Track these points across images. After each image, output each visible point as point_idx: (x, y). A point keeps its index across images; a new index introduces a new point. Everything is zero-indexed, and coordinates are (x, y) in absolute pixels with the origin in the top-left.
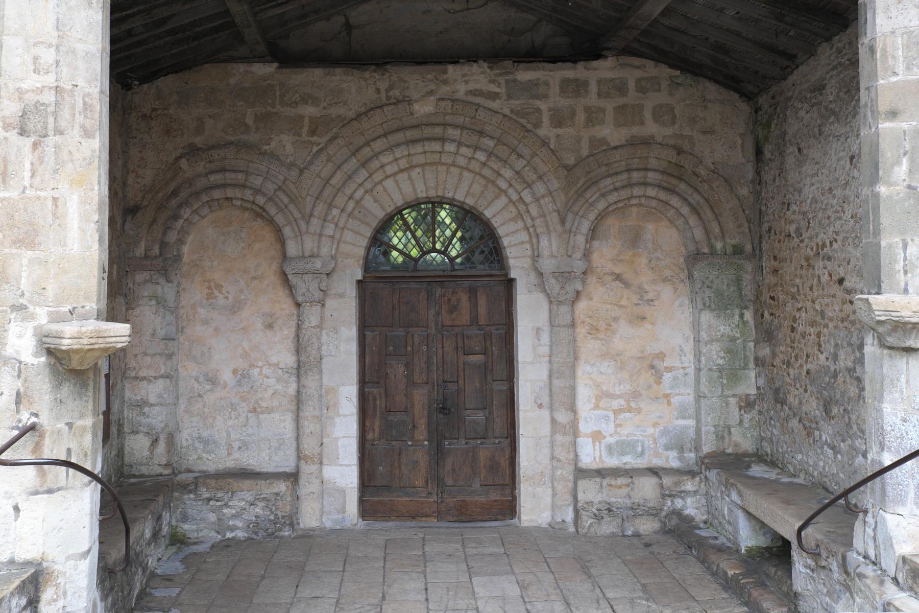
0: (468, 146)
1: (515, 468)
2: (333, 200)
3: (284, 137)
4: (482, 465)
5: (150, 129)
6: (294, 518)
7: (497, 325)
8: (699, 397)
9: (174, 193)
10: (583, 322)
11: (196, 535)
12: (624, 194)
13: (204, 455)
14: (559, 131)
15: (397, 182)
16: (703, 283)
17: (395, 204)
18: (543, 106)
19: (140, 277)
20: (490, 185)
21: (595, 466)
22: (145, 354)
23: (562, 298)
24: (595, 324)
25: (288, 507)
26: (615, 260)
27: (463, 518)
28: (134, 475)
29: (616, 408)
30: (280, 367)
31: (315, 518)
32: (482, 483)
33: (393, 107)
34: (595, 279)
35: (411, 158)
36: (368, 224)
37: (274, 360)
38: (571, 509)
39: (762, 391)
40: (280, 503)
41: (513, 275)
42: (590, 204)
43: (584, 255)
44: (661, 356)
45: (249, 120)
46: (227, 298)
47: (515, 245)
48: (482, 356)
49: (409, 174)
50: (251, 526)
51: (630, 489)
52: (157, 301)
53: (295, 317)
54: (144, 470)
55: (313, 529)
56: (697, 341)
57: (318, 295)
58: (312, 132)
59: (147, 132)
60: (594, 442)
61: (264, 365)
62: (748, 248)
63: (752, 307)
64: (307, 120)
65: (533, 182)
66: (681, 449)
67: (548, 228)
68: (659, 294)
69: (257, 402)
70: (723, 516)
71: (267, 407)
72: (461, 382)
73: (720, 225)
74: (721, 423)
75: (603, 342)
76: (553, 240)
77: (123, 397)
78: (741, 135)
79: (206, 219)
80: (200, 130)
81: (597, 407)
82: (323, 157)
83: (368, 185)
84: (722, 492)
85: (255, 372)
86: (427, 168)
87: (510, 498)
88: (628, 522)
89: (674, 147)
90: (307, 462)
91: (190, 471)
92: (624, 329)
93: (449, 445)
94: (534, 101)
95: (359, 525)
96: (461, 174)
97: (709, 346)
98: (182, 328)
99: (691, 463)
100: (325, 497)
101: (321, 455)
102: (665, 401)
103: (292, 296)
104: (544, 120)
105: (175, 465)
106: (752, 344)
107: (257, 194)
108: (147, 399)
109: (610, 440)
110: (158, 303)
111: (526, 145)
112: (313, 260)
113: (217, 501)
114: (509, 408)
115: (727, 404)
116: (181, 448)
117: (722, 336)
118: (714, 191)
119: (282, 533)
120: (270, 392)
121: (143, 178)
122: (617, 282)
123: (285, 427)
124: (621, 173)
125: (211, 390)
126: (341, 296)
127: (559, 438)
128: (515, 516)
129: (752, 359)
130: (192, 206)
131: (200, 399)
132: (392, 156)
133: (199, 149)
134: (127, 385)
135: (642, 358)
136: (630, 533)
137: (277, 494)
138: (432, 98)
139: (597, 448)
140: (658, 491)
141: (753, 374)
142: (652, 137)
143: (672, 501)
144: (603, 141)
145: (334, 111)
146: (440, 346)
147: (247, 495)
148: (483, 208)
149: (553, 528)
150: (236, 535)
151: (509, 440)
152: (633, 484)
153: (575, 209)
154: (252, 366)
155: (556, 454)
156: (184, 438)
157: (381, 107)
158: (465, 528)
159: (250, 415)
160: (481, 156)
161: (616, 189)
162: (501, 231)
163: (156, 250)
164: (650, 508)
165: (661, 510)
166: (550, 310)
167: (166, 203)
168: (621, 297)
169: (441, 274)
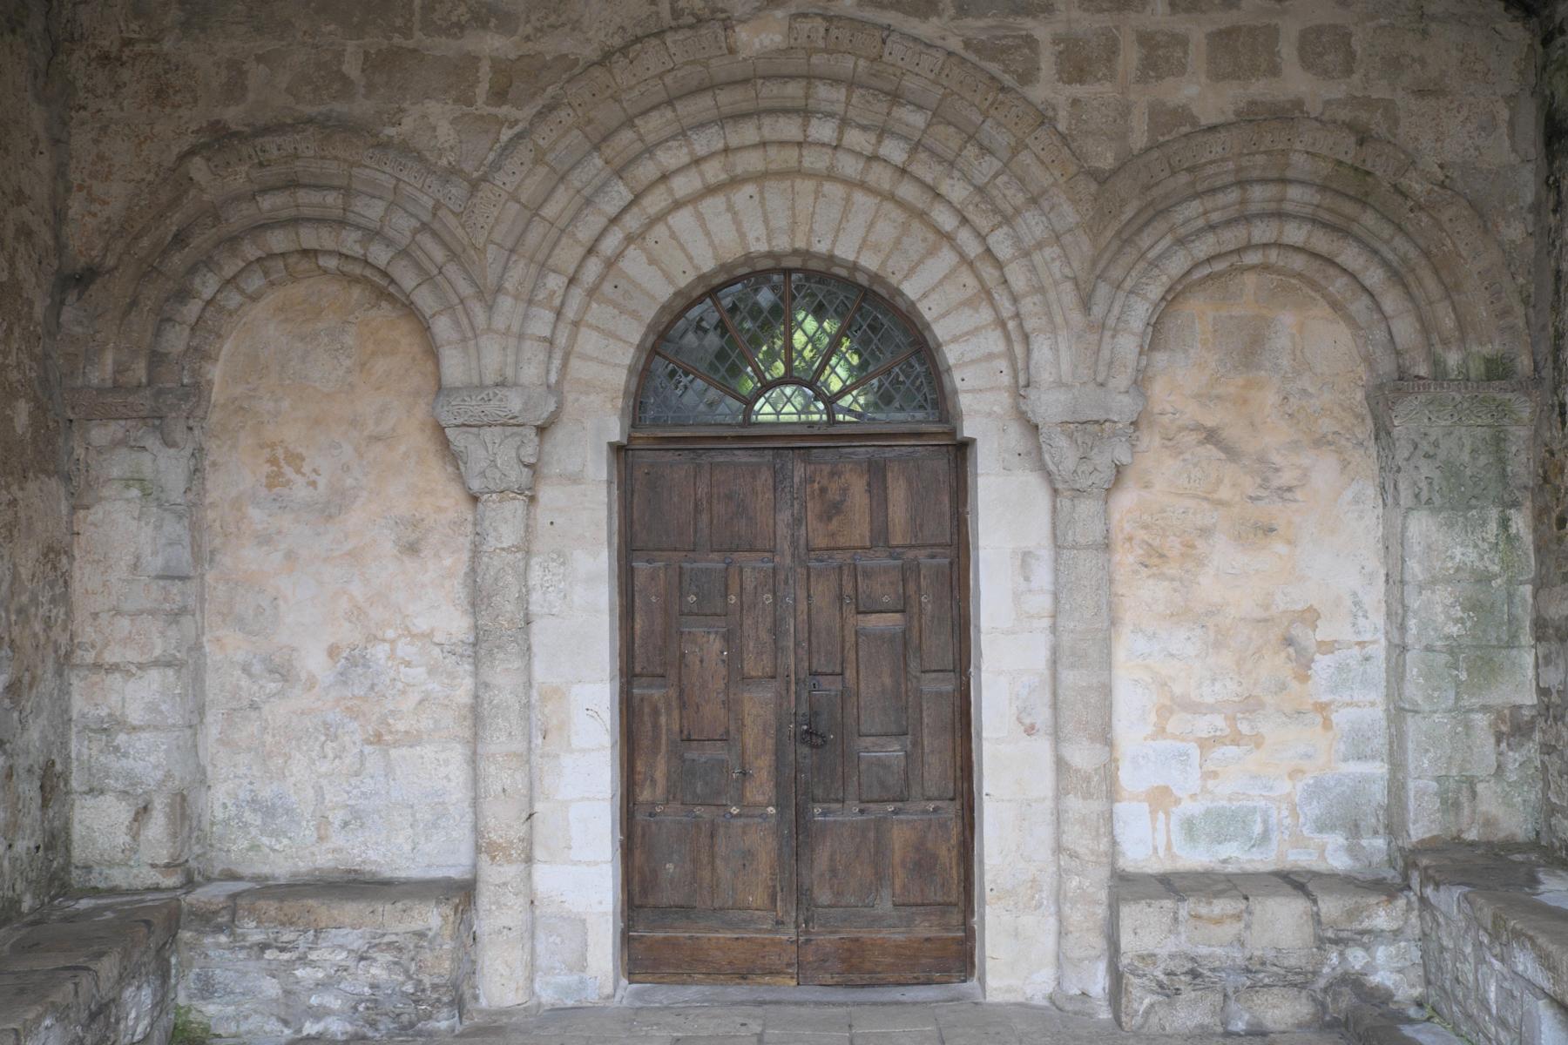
0: (864, 128)
1: (972, 866)
2: (549, 256)
3: (433, 107)
4: (897, 858)
5: (118, 87)
6: (465, 987)
7: (932, 546)
8: (1398, 712)
9: (180, 239)
10: (1130, 539)
11: (233, 1028)
12: (1232, 237)
13: (265, 840)
14: (1078, 90)
15: (700, 217)
16: (1416, 447)
17: (696, 268)
18: (1041, 31)
19: (100, 434)
20: (916, 224)
21: (1155, 867)
22: (117, 612)
23: (1083, 483)
24: (1156, 543)
25: (447, 964)
26: (1202, 398)
27: (855, 977)
28: (95, 888)
29: (1205, 735)
30: (436, 640)
31: (513, 986)
32: (899, 900)
33: (688, 33)
34: (1157, 441)
35: (731, 158)
36: (634, 314)
37: (422, 624)
38: (1101, 968)
39: (1555, 698)
40: (427, 956)
41: (967, 432)
42: (1150, 264)
43: (1135, 382)
44: (1310, 616)
45: (352, 68)
46: (313, 484)
47: (973, 362)
48: (898, 616)
49: (728, 200)
50: (361, 1008)
51: (1242, 925)
52: (143, 490)
53: (469, 528)
54: (119, 878)
55: (507, 1012)
56: (1396, 581)
57: (517, 476)
58: (500, 95)
59: (112, 96)
60: (1153, 812)
61: (400, 636)
62: (1524, 363)
63: (1528, 504)
64: (485, 70)
65: (1017, 211)
66: (1354, 830)
67: (1051, 320)
68: (1305, 474)
69: (383, 721)
70: (1484, 1003)
71: (407, 732)
72: (850, 674)
73: (1454, 309)
74: (1454, 772)
75: (1176, 584)
76: (1063, 347)
77: (66, 711)
78: (1509, 99)
79: (262, 303)
80: (235, 88)
81: (1161, 732)
82: (524, 153)
83: (632, 222)
84: (1478, 945)
85: (380, 652)
86: (772, 186)
87: (961, 934)
88: (1237, 1000)
89: (1350, 126)
90: (493, 858)
91: (232, 876)
92: (1223, 554)
93: (824, 814)
94: (1019, 20)
95: (617, 998)
96: (848, 200)
97: (1427, 594)
98: (212, 552)
99: (1376, 859)
100: (541, 935)
101: (528, 844)
102: (1319, 719)
103: (460, 478)
104: (1043, 66)
105: (193, 864)
106: (1527, 590)
107: (371, 240)
108: (122, 714)
109: (1189, 807)
110: (146, 494)
111: (999, 124)
112: (501, 392)
113: (282, 950)
114: (958, 741)
115: (1468, 727)
116: (213, 824)
117: (1458, 570)
118: (1442, 230)
119: (432, 1025)
120: (414, 697)
121: (105, 203)
122: (1209, 446)
123: (447, 778)
124: (1224, 188)
125: (280, 694)
126: (575, 479)
127: (1074, 804)
128: (972, 974)
129: (1527, 624)
130: (221, 268)
131: (254, 715)
132: (685, 150)
133: (235, 134)
134: (75, 681)
135: (1266, 620)
136: (1240, 1026)
137: (421, 935)
138: (779, 14)
139: (1161, 824)
140: (1308, 930)
141: (1528, 659)
142: (1298, 104)
143: (1341, 954)
144: (1182, 115)
145: (549, 46)
146: (802, 594)
147: (350, 938)
148: (899, 276)
149: (1061, 1010)
150: (326, 1029)
151: (958, 804)
152: (1250, 913)
153: (1116, 273)
154: (372, 639)
155: (1067, 840)
156: (219, 801)
157: (660, 34)
158: (860, 1004)
159: (368, 749)
160: (894, 151)
161: (1212, 228)
162: (941, 330)
163: (140, 371)
164: (1288, 970)
165: (1314, 973)
166: (1054, 510)
167: (160, 262)
168: (1219, 481)
169: (806, 431)
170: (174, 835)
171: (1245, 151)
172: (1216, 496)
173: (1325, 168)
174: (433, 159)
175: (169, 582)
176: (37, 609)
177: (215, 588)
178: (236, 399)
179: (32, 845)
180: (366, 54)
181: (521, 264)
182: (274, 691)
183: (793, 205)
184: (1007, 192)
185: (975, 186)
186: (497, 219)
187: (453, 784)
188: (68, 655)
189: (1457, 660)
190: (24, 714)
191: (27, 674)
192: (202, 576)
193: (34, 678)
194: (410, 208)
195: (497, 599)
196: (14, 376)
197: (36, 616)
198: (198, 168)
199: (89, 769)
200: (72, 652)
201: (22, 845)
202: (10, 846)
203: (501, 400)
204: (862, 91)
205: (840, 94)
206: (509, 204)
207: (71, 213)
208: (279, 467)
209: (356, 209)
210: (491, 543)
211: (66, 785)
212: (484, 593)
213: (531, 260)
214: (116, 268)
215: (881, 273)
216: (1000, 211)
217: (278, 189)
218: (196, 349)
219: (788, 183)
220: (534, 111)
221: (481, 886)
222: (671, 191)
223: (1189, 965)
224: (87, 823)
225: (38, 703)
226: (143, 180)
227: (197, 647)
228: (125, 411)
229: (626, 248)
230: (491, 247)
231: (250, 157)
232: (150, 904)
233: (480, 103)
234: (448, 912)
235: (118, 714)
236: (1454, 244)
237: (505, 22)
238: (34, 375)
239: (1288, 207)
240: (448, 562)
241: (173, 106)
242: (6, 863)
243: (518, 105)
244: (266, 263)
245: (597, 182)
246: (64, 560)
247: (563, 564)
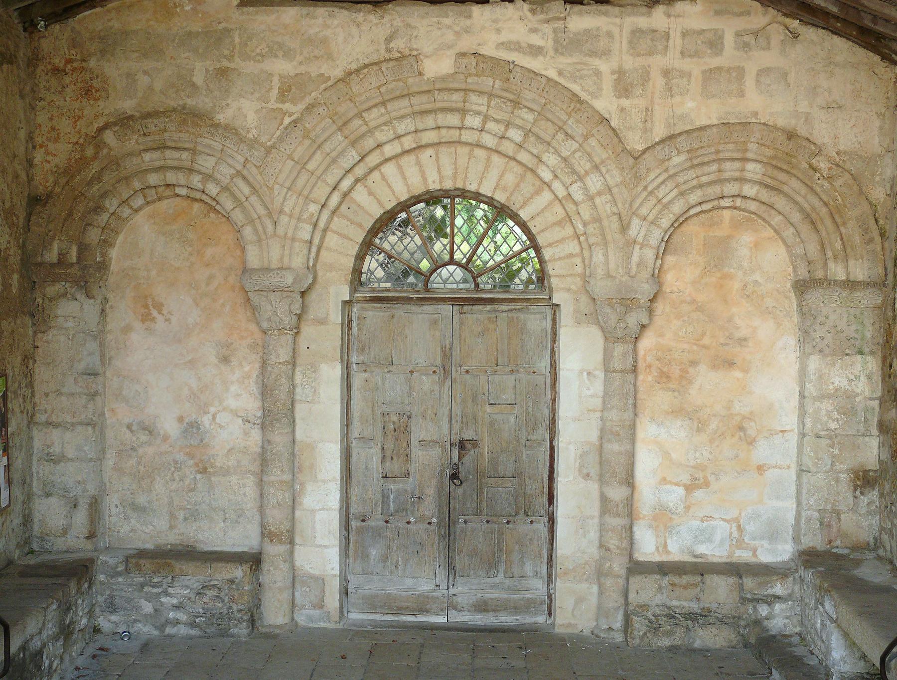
2: (310, 192)
10: (649, 366)
15: (400, 168)
17: (397, 198)
19: (51, 290)
20: (529, 175)
24: (665, 369)
36: (360, 225)
49: (417, 158)
51: (698, 589)
59: (60, 93)
64: (276, 79)
65: (587, 173)
71: (221, 467)
75: (676, 394)
79: (141, 213)
83: (359, 171)
86: (443, 150)
90: (272, 541)
96: (488, 159)
98: (110, 359)
101: (291, 532)
104: (604, 87)
113: (154, 587)
123: (244, 494)
131: (134, 454)
137: (232, 581)
140: (736, 596)
143: (755, 608)
145: (314, 70)
147: (192, 581)
148: (517, 206)
152: (703, 583)
159: (199, 476)
160: (515, 134)
164: (724, 616)
171: (722, 142)
172: (702, 343)
173: (769, 152)
174: (244, 134)
178: (125, 269)
180: (207, 71)
181: (294, 197)
183: (455, 162)
184: (580, 162)
185: (562, 157)
186: (280, 170)
189: (834, 442)
192: (105, 372)
194: (230, 161)
198: (109, 137)
200: (34, 415)
203: (281, 277)
204: (497, 100)
205: (484, 100)
208: (150, 310)
209: (200, 162)
210: (273, 359)
212: (268, 388)
215: (506, 204)
216: (576, 173)
217: (154, 149)
219: (453, 149)
220: (304, 107)
221: (265, 557)
222: (383, 154)
223: (668, 611)
227: (102, 414)
229: (355, 185)
233: (272, 102)
234: (247, 569)
236: (843, 200)
237: (288, 54)
239: (748, 175)
241: (95, 100)
243: (294, 102)
244: (145, 191)
245: (339, 149)
246: (31, 362)
247: (314, 372)
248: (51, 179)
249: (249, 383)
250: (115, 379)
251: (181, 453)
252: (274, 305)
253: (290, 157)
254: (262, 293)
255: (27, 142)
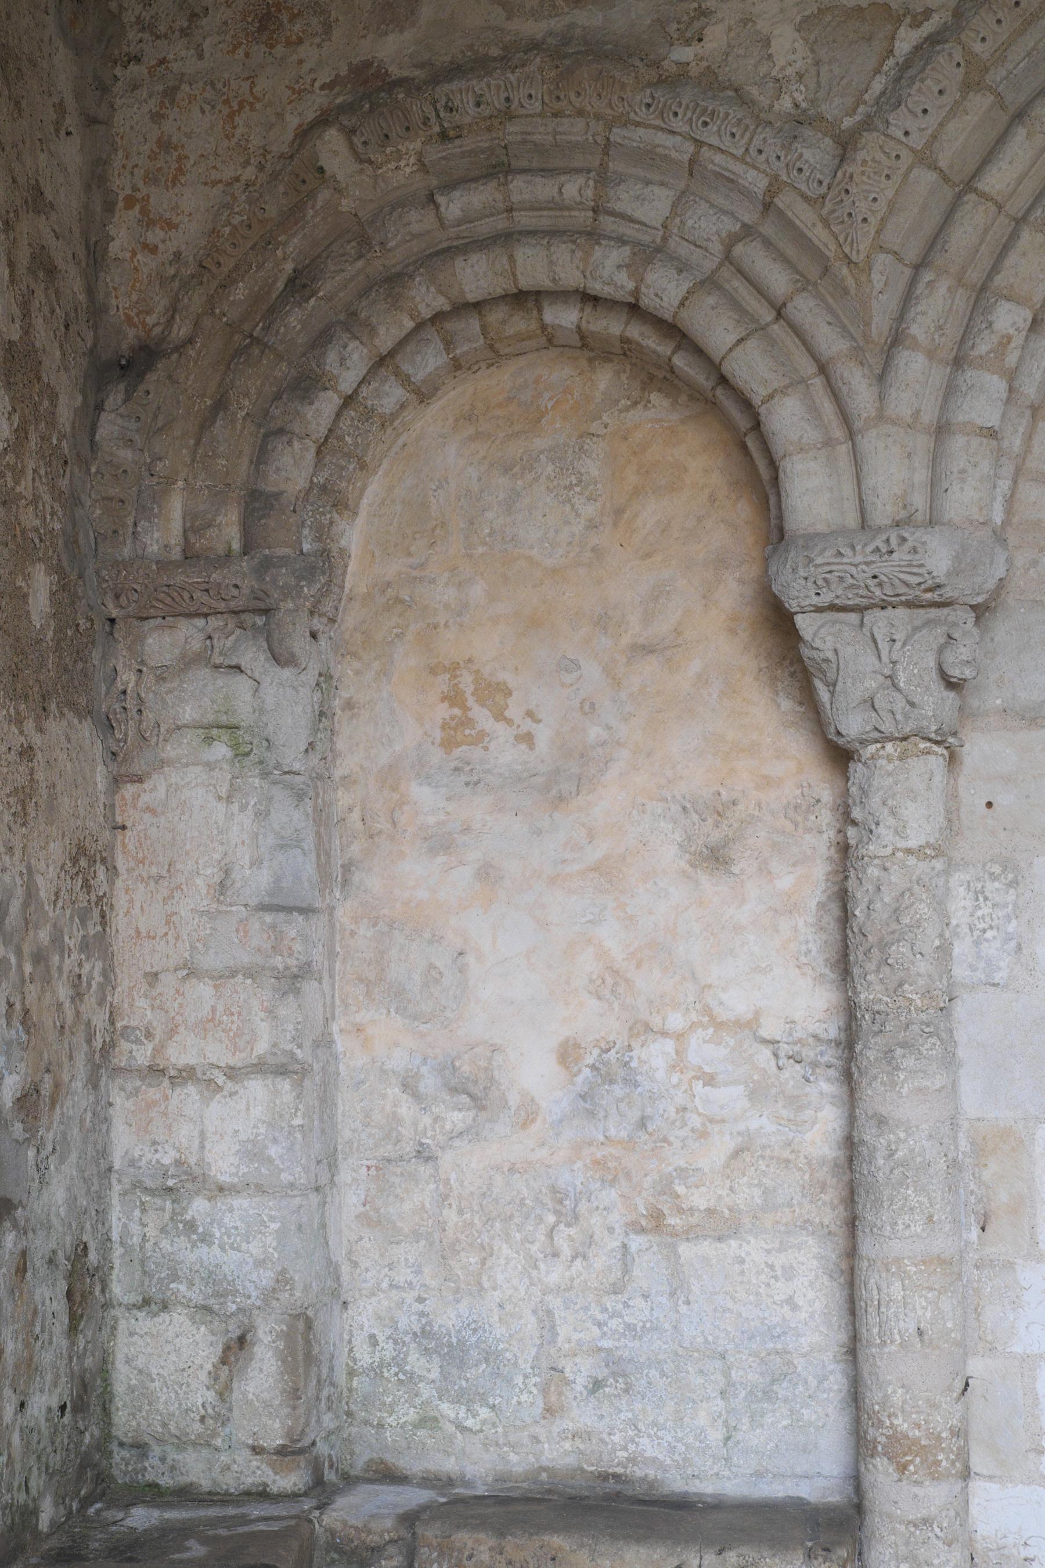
2: (995, 269)
5: (194, 16)
13: (446, 1408)
22: (191, 972)
30: (764, 1033)
46: (528, 739)
52: (235, 746)
59: (184, 33)
61: (693, 1026)
69: (665, 1187)
71: (710, 1212)
77: (104, 1152)
79: (435, 407)
90: (903, 1468)
98: (347, 868)
105: (322, 1449)
107: (648, 261)
108: (201, 1160)
110: (240, 754)
116: (351, 1373)
120: (722, 1145)
123: (790, 1301)
125: (471, 1133)
130: (373, 332)
131: (425, 1170)
134: (118, 1099)
159: (637, 1242)
167: (267, 329)
170: (295, 1394)
174: (764, 101)
175: (282, 916)
176: (62, 957)
177: (353, 933)
178: (389, 584)
179: (55, 1403)
181: (942, 289)
182: (461, 1126)
187: (804, 1315)
188: (108, 1049)
190: (44, 1154)
191: (47, 1077)
193: (57, 1086)
195: (900, 951)
196: (29, 519)
197: (60, 969)
199: (143, 1263)
200: (113, 1044)
201: (41, 1403)
202: (22, 1405)
203: (915, 550)
206: (915, 172)
207: (114, 248)
208: (466, 709)
209: (618, 207)
211: (103, 1291)
213: (960, 281)
214: (191, 341)
217: (475, 180)
218: (324, 489)
221: (875, 1522)
224: (140, 1362)
225: (64, 1134)
226: (237, 179)
227: (324, 1042)
228: (205, 598)
230: (882, 258)
231: (426, 121)
232: (262, 1527)
235: (192, 1160)
238: (57, 526)
240: (785, 882)
242: (16, 1439)
244: (449, 326)
247: (1014, 884)
248: (161, 302)
249: (796, 929)
250: (364, 931)
251: (579, 1164)
252: (885, 658)
253: (925, 158)
254: (842, 616)
255: (88, 188)
